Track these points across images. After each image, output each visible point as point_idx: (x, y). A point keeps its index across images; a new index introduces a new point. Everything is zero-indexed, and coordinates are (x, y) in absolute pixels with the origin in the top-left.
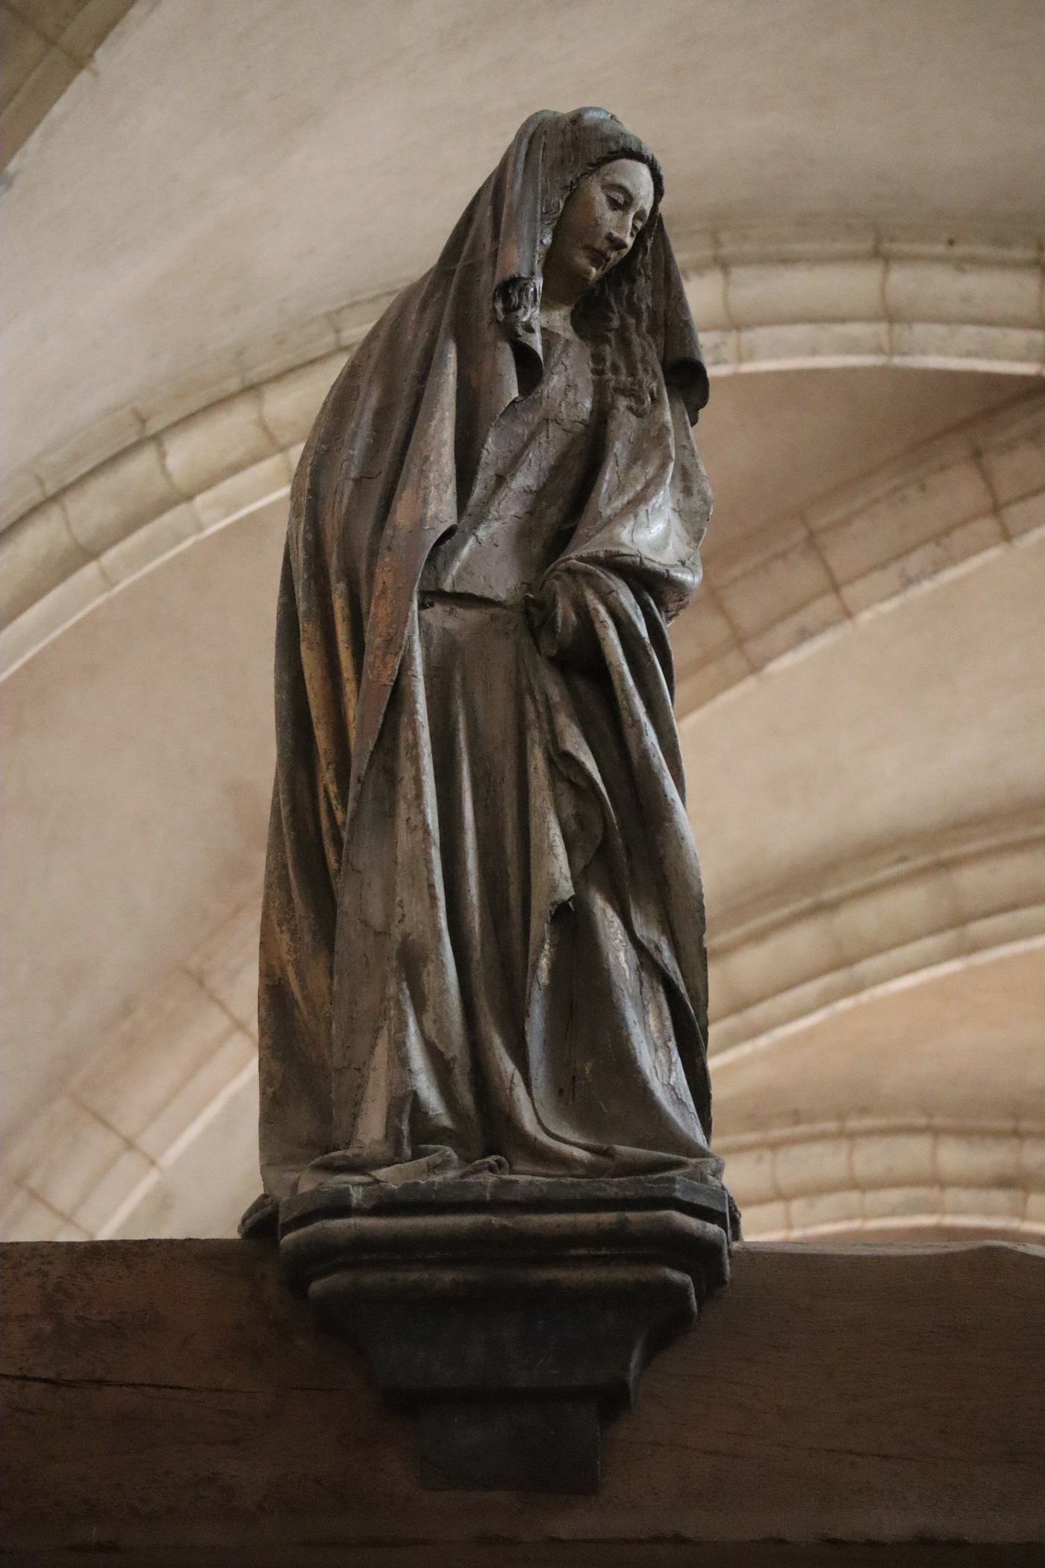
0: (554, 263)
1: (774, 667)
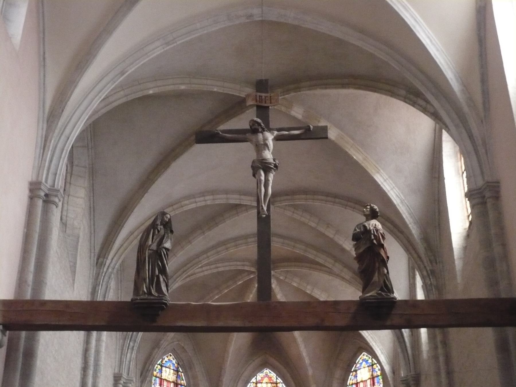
0: (161, 223)
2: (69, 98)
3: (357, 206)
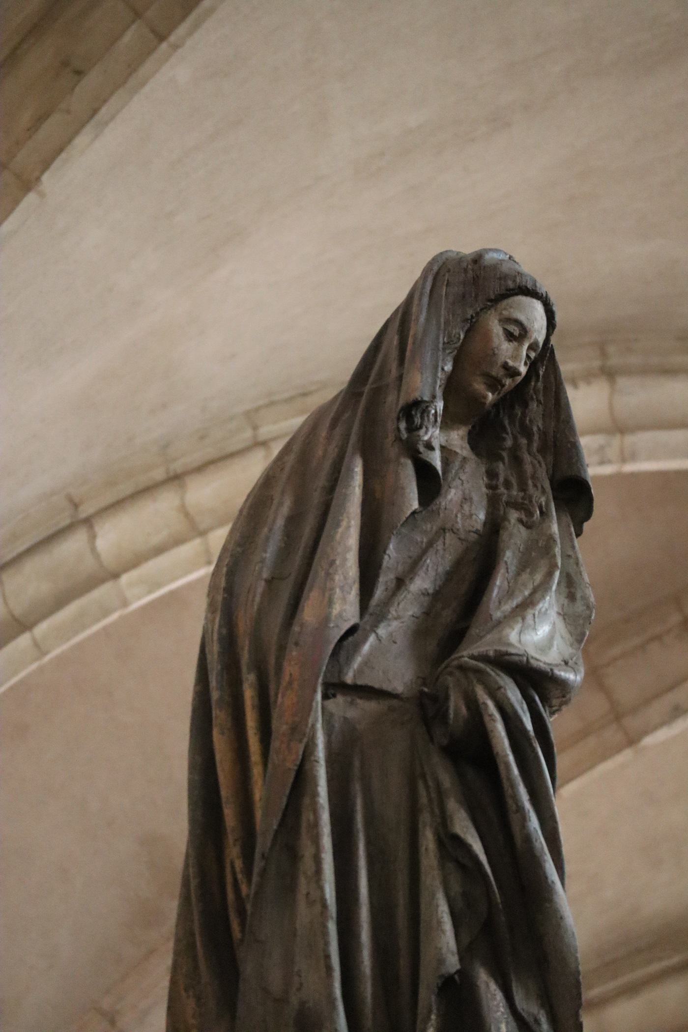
1: (648, 741)
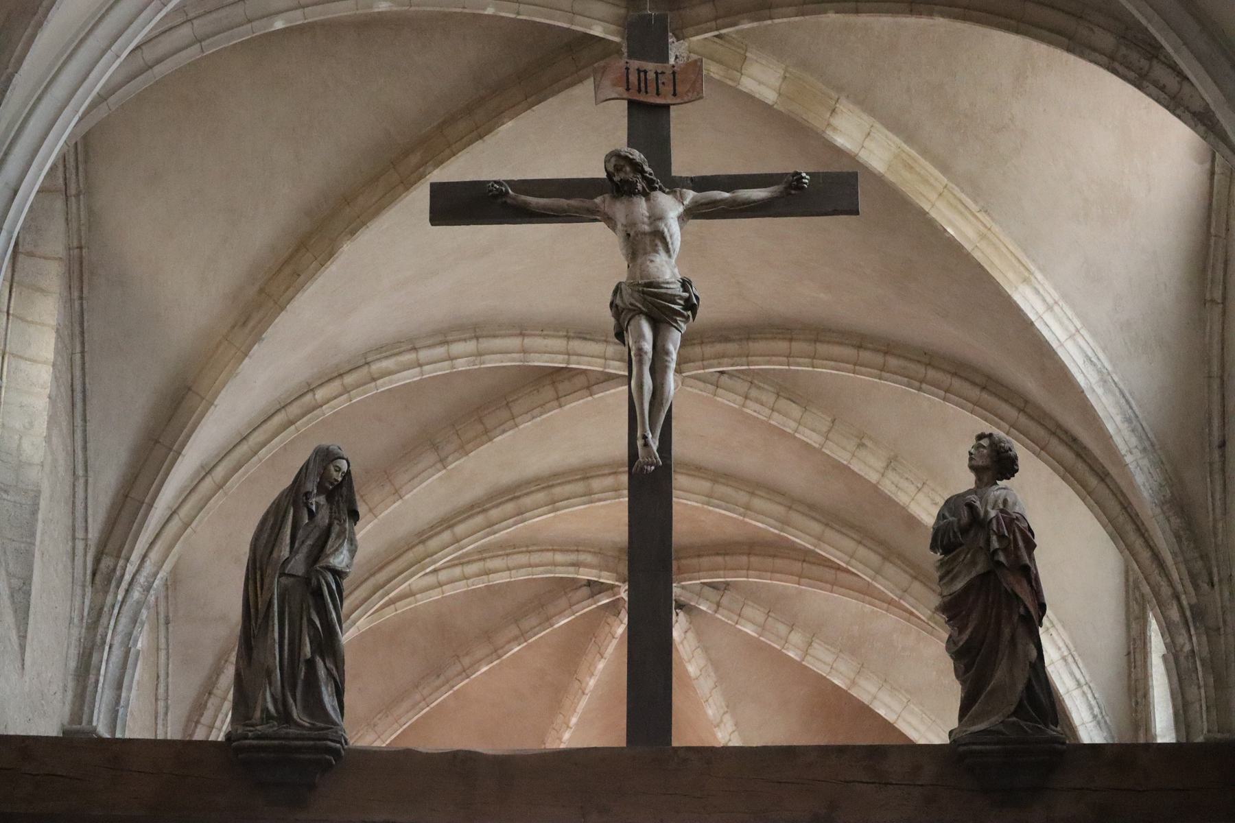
2: (20, 62)
3: (957, 383)
